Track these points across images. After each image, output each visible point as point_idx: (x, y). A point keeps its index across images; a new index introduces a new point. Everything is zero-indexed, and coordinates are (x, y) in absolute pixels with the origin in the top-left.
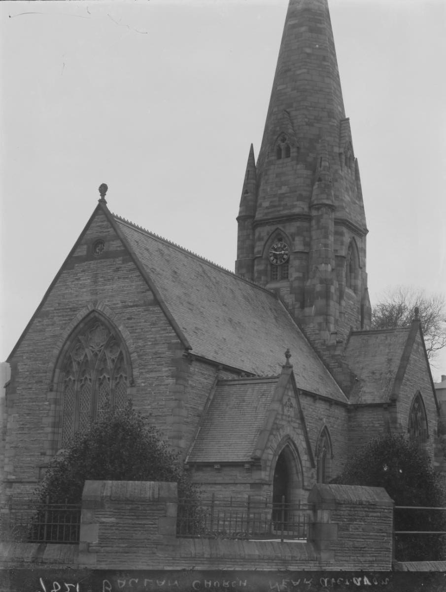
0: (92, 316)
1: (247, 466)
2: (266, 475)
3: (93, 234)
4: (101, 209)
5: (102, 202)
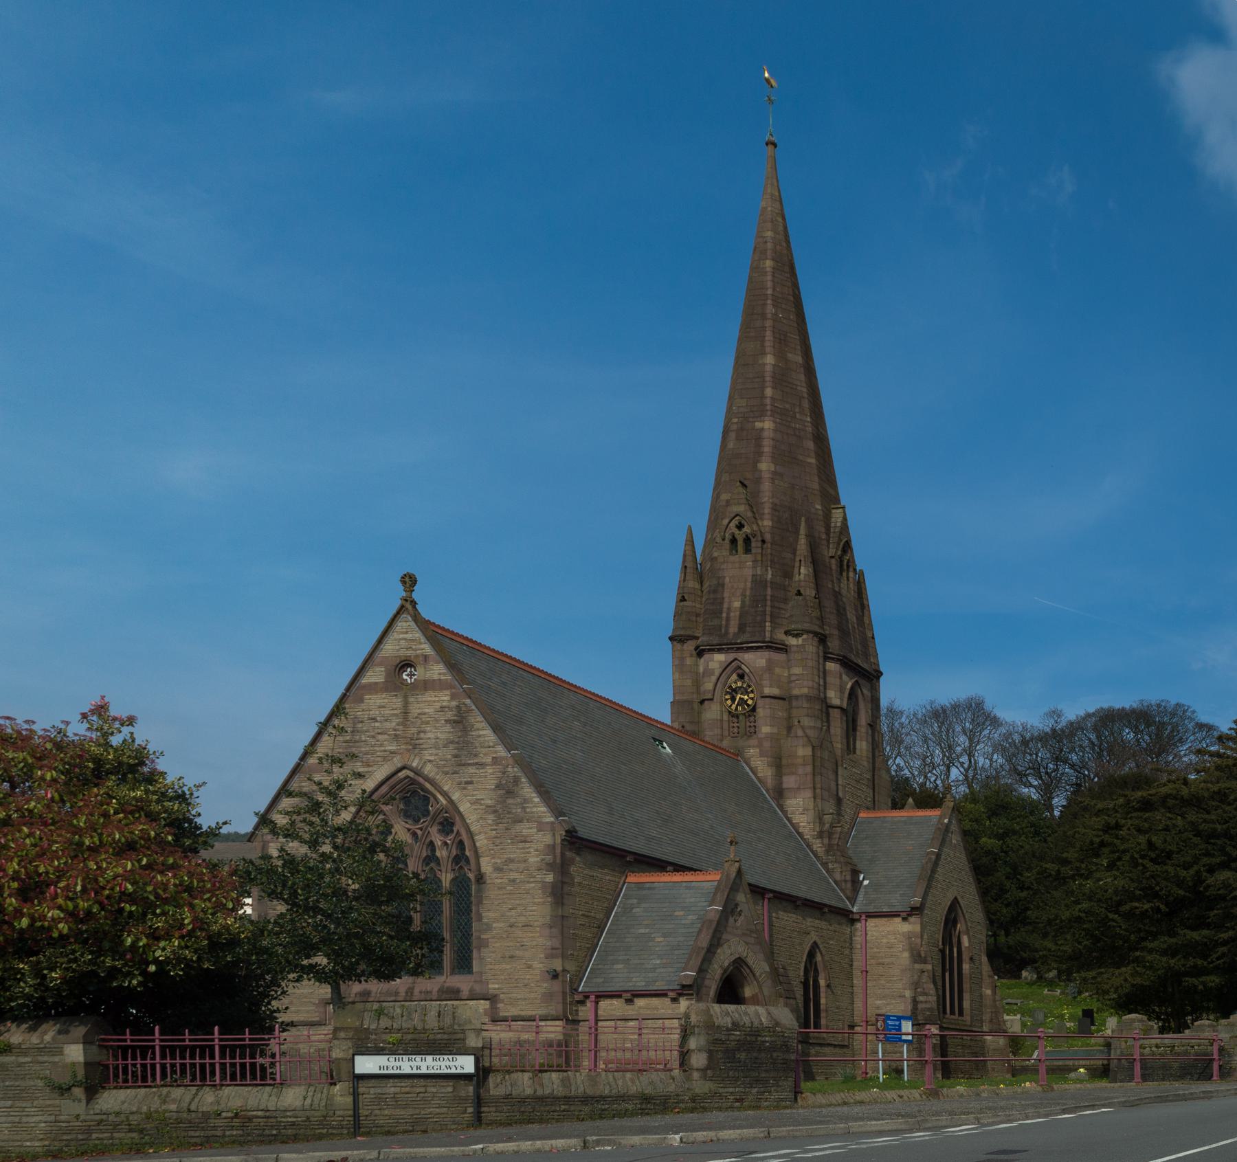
0: (401, 775)
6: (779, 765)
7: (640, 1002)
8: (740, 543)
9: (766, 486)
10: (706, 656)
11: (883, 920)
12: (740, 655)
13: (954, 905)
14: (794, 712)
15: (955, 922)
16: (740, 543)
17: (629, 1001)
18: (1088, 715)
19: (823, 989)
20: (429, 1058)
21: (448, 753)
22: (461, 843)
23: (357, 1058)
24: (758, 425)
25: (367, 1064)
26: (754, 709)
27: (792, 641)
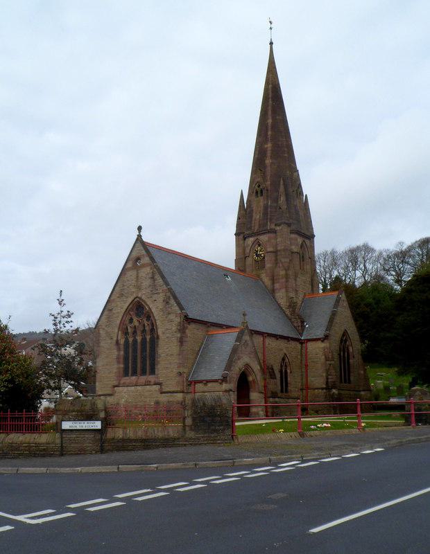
0: (136, 300)
1: (220, 381)
2: (232, 385)
3: (134, 254)
4: (139, 238)
5: (139, 236)
6: (273, 280)
7: (209, 385)
8: (259, 192)
9: (269, 169)
10: (247, 240)
11: (314, 342)
12: (258, 237)
13: (345, 333)
14: (278, 257)
15: (346, 341)
16: (259, 192)
17: (206, 384)
18: (416, 242)
19: (289, 374)
20: (86, 422)
21: (148, 290)
22: (153, 323)
23: (63, 422)
24: (266, 146)
25: (66, 425)
26: (264, 257)
27: (278, 228)
